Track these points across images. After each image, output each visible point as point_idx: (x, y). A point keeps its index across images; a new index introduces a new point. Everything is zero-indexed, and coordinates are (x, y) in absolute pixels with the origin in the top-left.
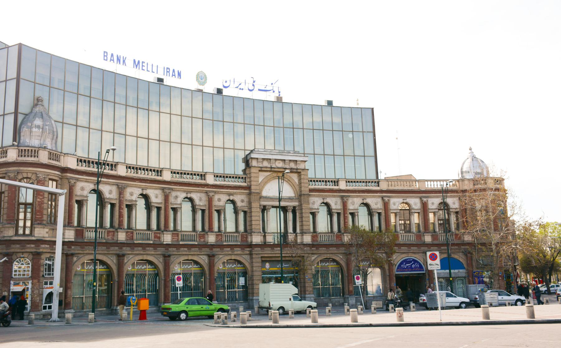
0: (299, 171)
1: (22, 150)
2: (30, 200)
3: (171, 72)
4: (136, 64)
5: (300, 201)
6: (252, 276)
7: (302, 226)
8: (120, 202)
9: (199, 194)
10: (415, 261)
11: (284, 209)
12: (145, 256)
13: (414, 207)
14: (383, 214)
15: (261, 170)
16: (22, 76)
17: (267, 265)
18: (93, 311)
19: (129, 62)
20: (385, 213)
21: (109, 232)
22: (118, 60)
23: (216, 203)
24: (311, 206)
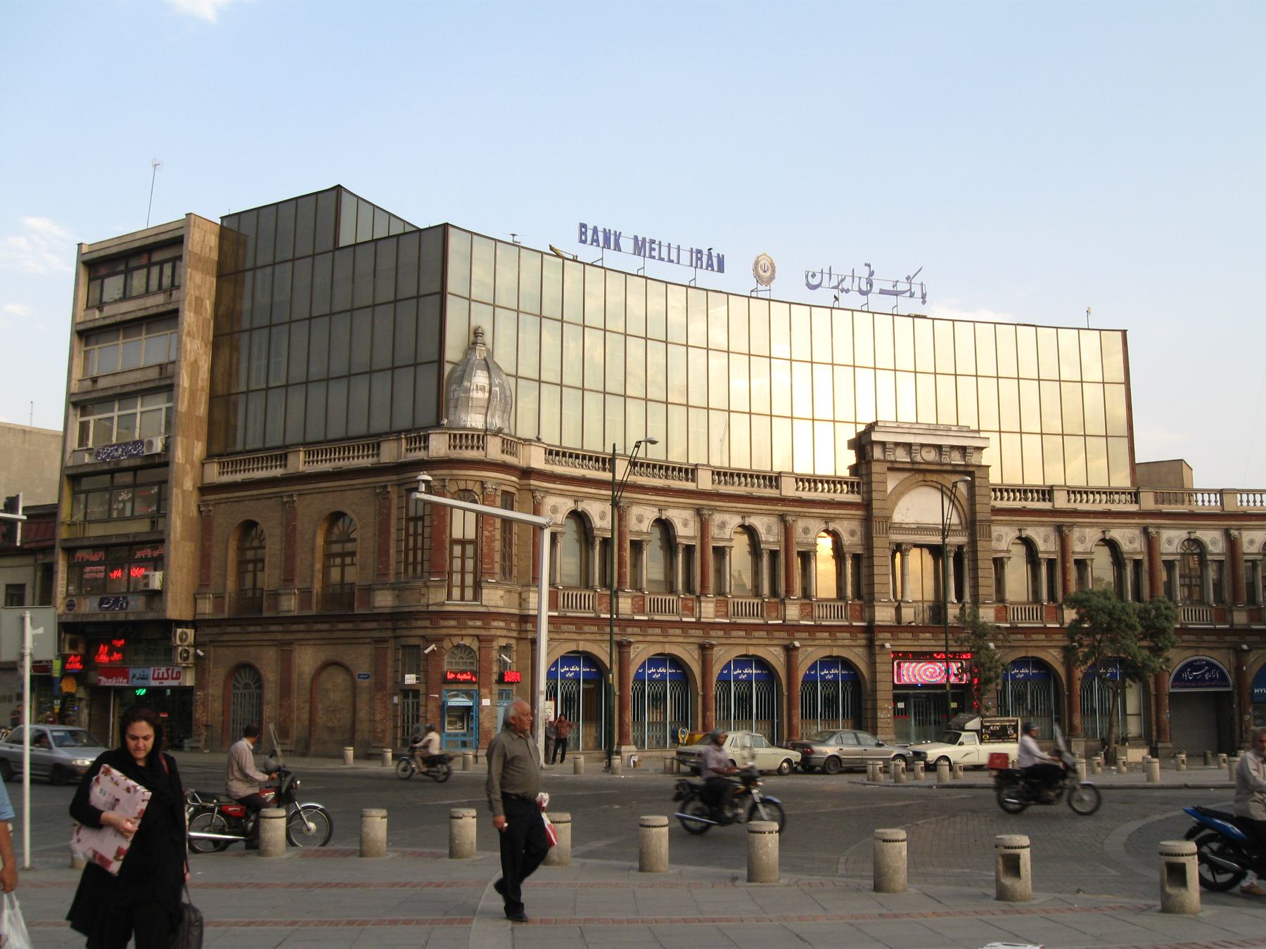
0: (970, 469)
1: (455, 436)
2: (471, 534)
4: (640, 247)
9: (766, 519)
10: (1212, 666)
12: (667, 646)
13: (1211, 548)
14: (1146, 565)
15: (894, 468)
22: (607, 240)
24: (994, 544)
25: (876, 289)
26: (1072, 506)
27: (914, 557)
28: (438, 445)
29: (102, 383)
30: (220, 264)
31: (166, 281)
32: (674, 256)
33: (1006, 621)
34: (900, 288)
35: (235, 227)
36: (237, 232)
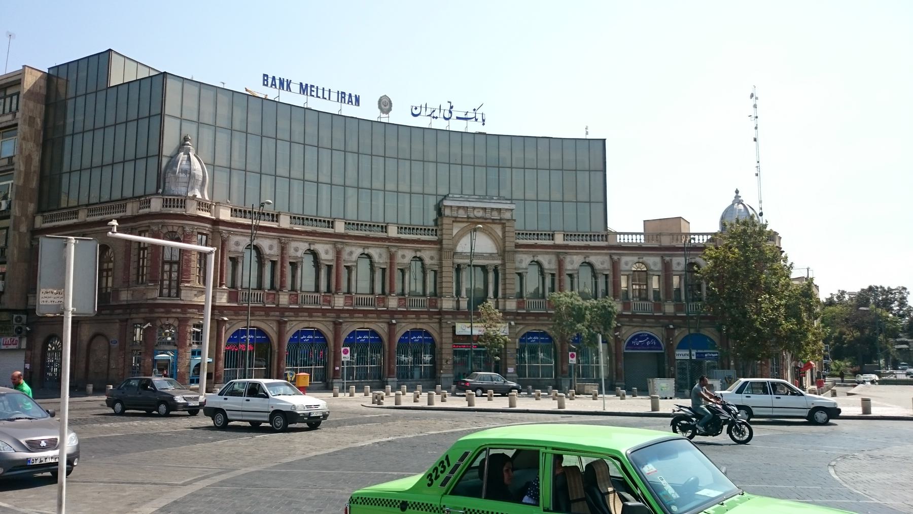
3: (347, 97)
5: (503, 259)
6: (441, 349)
7: (504, 289)
9: (378, 250)
15: (456, 220)
19: (295, 88)
22: (281, 83)
23: (398, 259)
24: (517, 265)
25: (454, 117)
26: (566, 243)
28: (156, 205)
30: (47, 97)
32: (326, 95)
33: (524, 309)
34: (469, 116)
35: (55, 74)
36: (52, 78)
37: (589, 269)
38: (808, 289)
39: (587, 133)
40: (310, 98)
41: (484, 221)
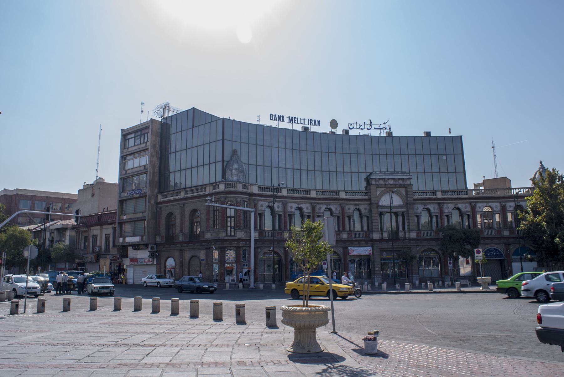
2: (233, 214)
3: (313, 122)
4: (291, 120)
5: (407, 208)
6: (374, 261)
7: (409, 225)
8: (285, 213)
9: (335, 206)
11: (396, 214)
14: (471, 216)
15: (378, 186)
16: (225, 138)
17: (385, 254)
18: (274, 283)
19: (286, 120)
20: (473, 214)
21: (278, 233)
22: (279, 118)
23: (347, 211)
24: (415, 211)
25: (373, 128)
27: (387, 216)
28: (222, 187)
29: (129, 172)
30: (162, 133)
31: (146, 140)
34: (381, 127)
37: (457, 211)
38: (97, 188)
39: (450, 133)
40: (294, 124)
41: (395, 186)
